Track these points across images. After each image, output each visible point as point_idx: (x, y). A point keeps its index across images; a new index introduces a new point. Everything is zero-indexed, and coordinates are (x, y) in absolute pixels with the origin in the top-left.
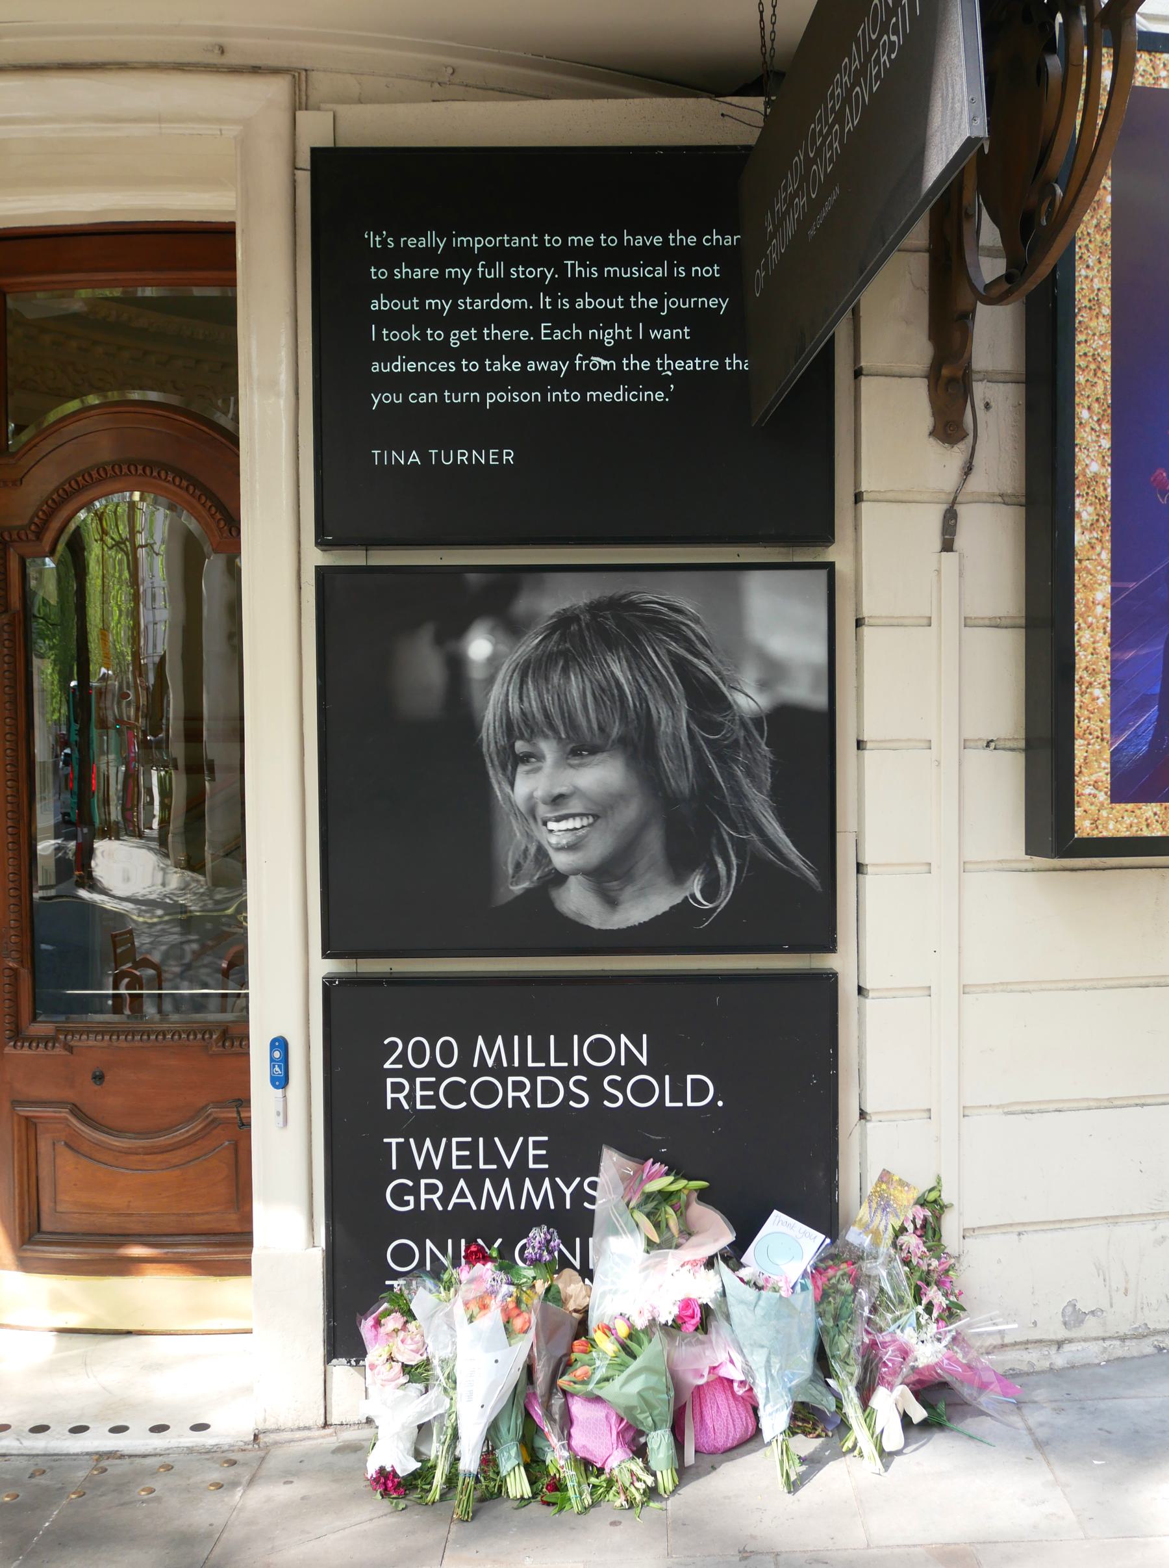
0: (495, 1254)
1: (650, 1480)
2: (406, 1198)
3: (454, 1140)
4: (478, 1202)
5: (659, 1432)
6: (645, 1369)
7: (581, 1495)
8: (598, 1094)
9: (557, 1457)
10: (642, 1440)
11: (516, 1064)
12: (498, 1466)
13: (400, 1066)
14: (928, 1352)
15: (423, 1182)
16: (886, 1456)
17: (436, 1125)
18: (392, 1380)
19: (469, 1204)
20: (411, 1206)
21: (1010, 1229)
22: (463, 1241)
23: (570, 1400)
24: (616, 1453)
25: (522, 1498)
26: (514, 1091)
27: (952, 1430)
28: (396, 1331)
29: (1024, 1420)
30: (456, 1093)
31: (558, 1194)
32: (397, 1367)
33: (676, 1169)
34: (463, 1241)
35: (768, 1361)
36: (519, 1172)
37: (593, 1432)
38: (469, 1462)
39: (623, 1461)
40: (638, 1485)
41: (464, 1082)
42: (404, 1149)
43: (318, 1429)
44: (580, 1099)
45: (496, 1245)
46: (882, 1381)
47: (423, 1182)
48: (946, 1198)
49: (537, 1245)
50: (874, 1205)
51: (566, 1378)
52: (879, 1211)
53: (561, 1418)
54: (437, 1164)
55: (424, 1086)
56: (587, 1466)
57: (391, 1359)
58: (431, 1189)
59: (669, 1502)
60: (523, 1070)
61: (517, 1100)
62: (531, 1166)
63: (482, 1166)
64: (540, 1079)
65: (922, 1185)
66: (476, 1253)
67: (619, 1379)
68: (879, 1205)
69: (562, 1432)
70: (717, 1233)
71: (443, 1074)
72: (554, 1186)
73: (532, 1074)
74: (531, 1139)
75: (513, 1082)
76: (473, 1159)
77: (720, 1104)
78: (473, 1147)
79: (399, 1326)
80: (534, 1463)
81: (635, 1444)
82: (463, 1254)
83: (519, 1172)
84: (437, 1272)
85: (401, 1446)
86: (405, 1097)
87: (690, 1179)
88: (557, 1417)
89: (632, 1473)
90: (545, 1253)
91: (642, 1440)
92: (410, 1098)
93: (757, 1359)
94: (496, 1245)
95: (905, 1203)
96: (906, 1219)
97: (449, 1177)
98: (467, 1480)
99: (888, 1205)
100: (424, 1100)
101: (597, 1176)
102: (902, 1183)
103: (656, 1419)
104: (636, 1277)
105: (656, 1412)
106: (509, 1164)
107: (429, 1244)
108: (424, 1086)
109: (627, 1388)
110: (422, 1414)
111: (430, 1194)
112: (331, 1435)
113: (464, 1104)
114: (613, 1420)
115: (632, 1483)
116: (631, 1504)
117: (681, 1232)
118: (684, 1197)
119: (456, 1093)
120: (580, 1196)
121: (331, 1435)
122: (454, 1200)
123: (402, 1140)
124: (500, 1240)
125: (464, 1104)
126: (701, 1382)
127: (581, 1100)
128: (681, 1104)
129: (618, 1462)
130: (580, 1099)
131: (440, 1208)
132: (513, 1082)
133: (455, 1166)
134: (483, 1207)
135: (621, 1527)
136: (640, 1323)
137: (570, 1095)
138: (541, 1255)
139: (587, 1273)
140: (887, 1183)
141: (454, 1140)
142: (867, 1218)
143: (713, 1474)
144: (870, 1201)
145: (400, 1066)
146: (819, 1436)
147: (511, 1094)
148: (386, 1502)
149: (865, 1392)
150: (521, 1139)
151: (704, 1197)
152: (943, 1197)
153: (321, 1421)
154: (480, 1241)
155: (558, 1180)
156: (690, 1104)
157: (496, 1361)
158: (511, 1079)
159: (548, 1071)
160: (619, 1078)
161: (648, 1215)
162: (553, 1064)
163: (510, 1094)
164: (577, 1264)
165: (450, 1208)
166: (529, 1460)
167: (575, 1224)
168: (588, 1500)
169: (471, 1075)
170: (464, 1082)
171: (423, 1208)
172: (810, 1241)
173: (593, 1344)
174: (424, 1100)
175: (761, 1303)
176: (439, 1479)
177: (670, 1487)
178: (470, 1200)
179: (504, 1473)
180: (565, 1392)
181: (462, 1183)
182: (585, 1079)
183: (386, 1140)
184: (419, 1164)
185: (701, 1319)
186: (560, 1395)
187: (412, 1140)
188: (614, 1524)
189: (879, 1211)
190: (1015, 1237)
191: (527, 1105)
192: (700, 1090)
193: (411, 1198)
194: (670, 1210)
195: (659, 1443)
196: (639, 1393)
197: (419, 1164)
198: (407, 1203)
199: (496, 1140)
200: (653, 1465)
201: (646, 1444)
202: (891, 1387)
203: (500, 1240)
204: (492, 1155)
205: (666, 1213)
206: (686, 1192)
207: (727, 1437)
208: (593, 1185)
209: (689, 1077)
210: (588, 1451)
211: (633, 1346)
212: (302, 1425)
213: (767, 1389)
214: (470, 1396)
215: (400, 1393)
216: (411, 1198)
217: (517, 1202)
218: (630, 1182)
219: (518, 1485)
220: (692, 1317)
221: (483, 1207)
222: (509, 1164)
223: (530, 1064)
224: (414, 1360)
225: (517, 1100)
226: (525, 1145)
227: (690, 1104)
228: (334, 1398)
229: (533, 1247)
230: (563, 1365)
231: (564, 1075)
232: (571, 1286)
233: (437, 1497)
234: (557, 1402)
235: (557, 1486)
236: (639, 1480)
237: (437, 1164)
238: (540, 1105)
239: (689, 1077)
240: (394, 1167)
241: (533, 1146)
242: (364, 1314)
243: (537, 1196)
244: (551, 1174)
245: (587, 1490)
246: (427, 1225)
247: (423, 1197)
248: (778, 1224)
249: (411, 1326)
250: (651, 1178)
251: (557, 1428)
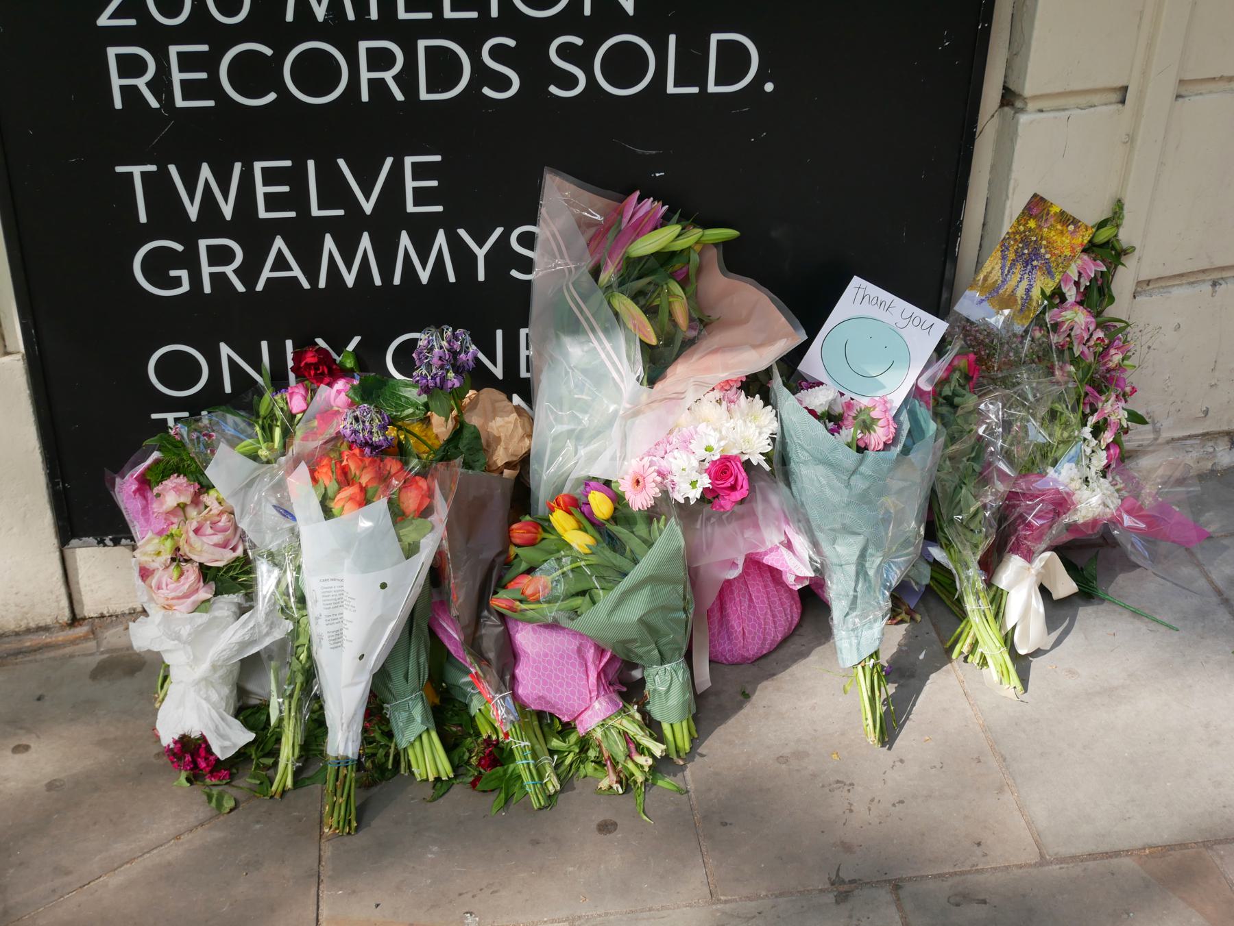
0: (349, 363)
1: (658, 749)
2: (173, 273)
3: (258, 166)
4: (313, 277)
5: (668, 666)
6: (651, 580)
7: (541, 777)
8: (538, 72)
9: (492, 711)
10: (637, 674)
11: (374, 15)
12: (388, 721)
13: (132, 22)
14: (1093, 502)
15: (203, 244)
16: (1022, 664)
17: (220, 137)
18: (186, 596)
19: (296, 278)
20: (185, 287)
21: (1202, 277)
22: (289, 344)
23: (511, 625)
24: (597, 705)
25: (438, 779)
26: (370, 69)
27: (1102, 600)
28: (182, 507)
29: (1206, 576)
30: (253, 74)
31: (463, 257)
32: (192, 574)
33: (685, 211)
34: (289, 344)
35: (863, 556)
36: (388, 222)
37: (552, 667)
38: (343, 740)
39: (609, 717)
40: (641, 760)
41: (268, 52)
42: (158, 186)
43: (63, 627)
44: (502, 83)
45: (351, 347)
46: (1016, 549)
47: (203, 244)
48: (1125, 236)
49: (435, 361)
50: (1011, 255)
51: (503, 594)
52: (1019, 266)
53: (499, 656)
54: (227, 211)
55: (187, 62)
56: (546, 723)
57: (178, 558)
58: (220, 256)
59: (688, 773)
60: (388, 26)
61: (377, 86)
62: (411, 208)
63: (315, 212)
64: (422, 44)
65: (1090, 214)
66: (316, 366)
67: (606, 599)
68: (1019, 255)
69: (502, 678)
70: (765, 334)
71: (223, 38)
72: (456, 245)
73: (407, 35)
74: (409, 161)
75: (369, 51)
76: (298, 199)
77: (769, 87)
78: (296, 177)
79: (186, 499)
80: (449, 716)
81: (625, 684)
82: (290, 364)
83: (388, 222)
84: (243, 398)
85: (215, 697)
86: (148, 84)
87: (705, 226)
88: (491, 655)
89: (625, 735)
90: (451, 375)
91: (637, 674)
92: (161, 84)
93: (844, 551)
94: (351, 347)
95: (1067, 252)
96: (1066, 278)
97: (254, 235)
98: (343, 771)
99: (1036, 254)
100: (190, 90)
101: (534, 223)
102: (1066, 219)
103: (665, 649)
104: (623, 419)
105: (663, 641)
106: (368, 207)
107: (225, 350)
108: (187, 62)
109: (621, 611)
110: (244, 645)
111: (217, 267)
112: (85, 638)
113: (272, 96)
114: (590, 654)
115: (630, 756)
116: (626, 782)
117: (691, 319)
118: (695, 257)
119: (253, 74)
120: (502, 257)
121: (85, 638)
122: (266, 273)
123: (152, 168)
124: (356, 340)
125: (272, 96)
126: (733, 574)
127: (504, 83)
128: (695, 90)
129: (597, 715)
130: (502, 83)
131: (240, 288)
132: (369, 51)
133: (263, 214)
134: (322, 284)
135: (618, 835)
136: (639, 501)
137: (482, 75)
138: (444, 379)
139: (518, 385)
140: (1038, 218)
141: (258, 166)
142: (996, 275)
143: (747, 709)
144: (1005, 248)
145: (132, 22)
146: (902, 621)
147: (365, 75)
148: (198, 792)
149: (990, 564)
150: (389, 161)
151: (736, 260)
152: (1121, 236)
153: (66, 615)
154: (321, 342)
155: (462, 232)
156: (712, 88)
157: (384, 586)
158: (363, 46)
159: (439, 27)
160: (579, 41)
161: (635, 297)
162: (448, 14)
163: (365, 73)
164: (498, 372)
165: (260, 287)
166: (437, 701)
167: (495, 308)
168: (553, 784)
169: (283, 38)
170: (268, 52)
171: (207, 289)
172: (921, 331)
173: (545, 526)
174: (190, 90)
175: (863, 469)
176: (287, 752)
177: (686, 745)
178: (297, 272)
179: (403, 744)
180: (502, 617)
181: (279, 243)
182: (511, 43)
183: (119, 169)
184: (193, 212)
185: (734, 484)
186: (495, 620)
187: (172, 169)
188: (606, 827)
189: (1019, 266)
190: (1207, 288)
191: (399, 96)
192: (733, 62)
193: (184, 274)
194: (676, 288)
195: (666, 686)
196: (641, 621)
197: (193, 212)
198: (177, 282)
199: (341, 163)
200: (656, 710)
201: (642, 682)
202: (1029, 556)
203: (356, 340)
204: (334, 191)
205: (670, 293)
206: (698, 248)
207: (763, 644)
208: (528, 240)
209: (715, 38)
210: (548, 702)
211: (619, 531)
212: (32, 625)
213: (855, 597)
214: (337, 640)
215: (201, 618)
216: (184, 274)
217: (387, 270)
218: (600, 237)
219: (429, 759)
220: (733, 488)
221: (322, 284)
222: (368, 207)
223: (402, 15)
224: (222, 558)
225: (377, 86)
226: (397, 174)
227: (712, 88)
228: (84, 589)
229: (429, 365)
230: (497, 573)
231: (471, 36)
232: (499, 422)
233: (289, 783)
234: (491, 630)
235: (497, 755)
236: (641, 750)
237: (227, 211)
238: (424, 96)
239: (715, 38)
240: (143, 218)
241: (413, 175)
242: (119, 468)
243: (424, 262)
244: (449, 222)
245: (548, 764)
246: (212, 317)
247: (206, 270)
248: (862, 303)
249: (209, 499)
250: (639, 230)
251: (493, 675)
